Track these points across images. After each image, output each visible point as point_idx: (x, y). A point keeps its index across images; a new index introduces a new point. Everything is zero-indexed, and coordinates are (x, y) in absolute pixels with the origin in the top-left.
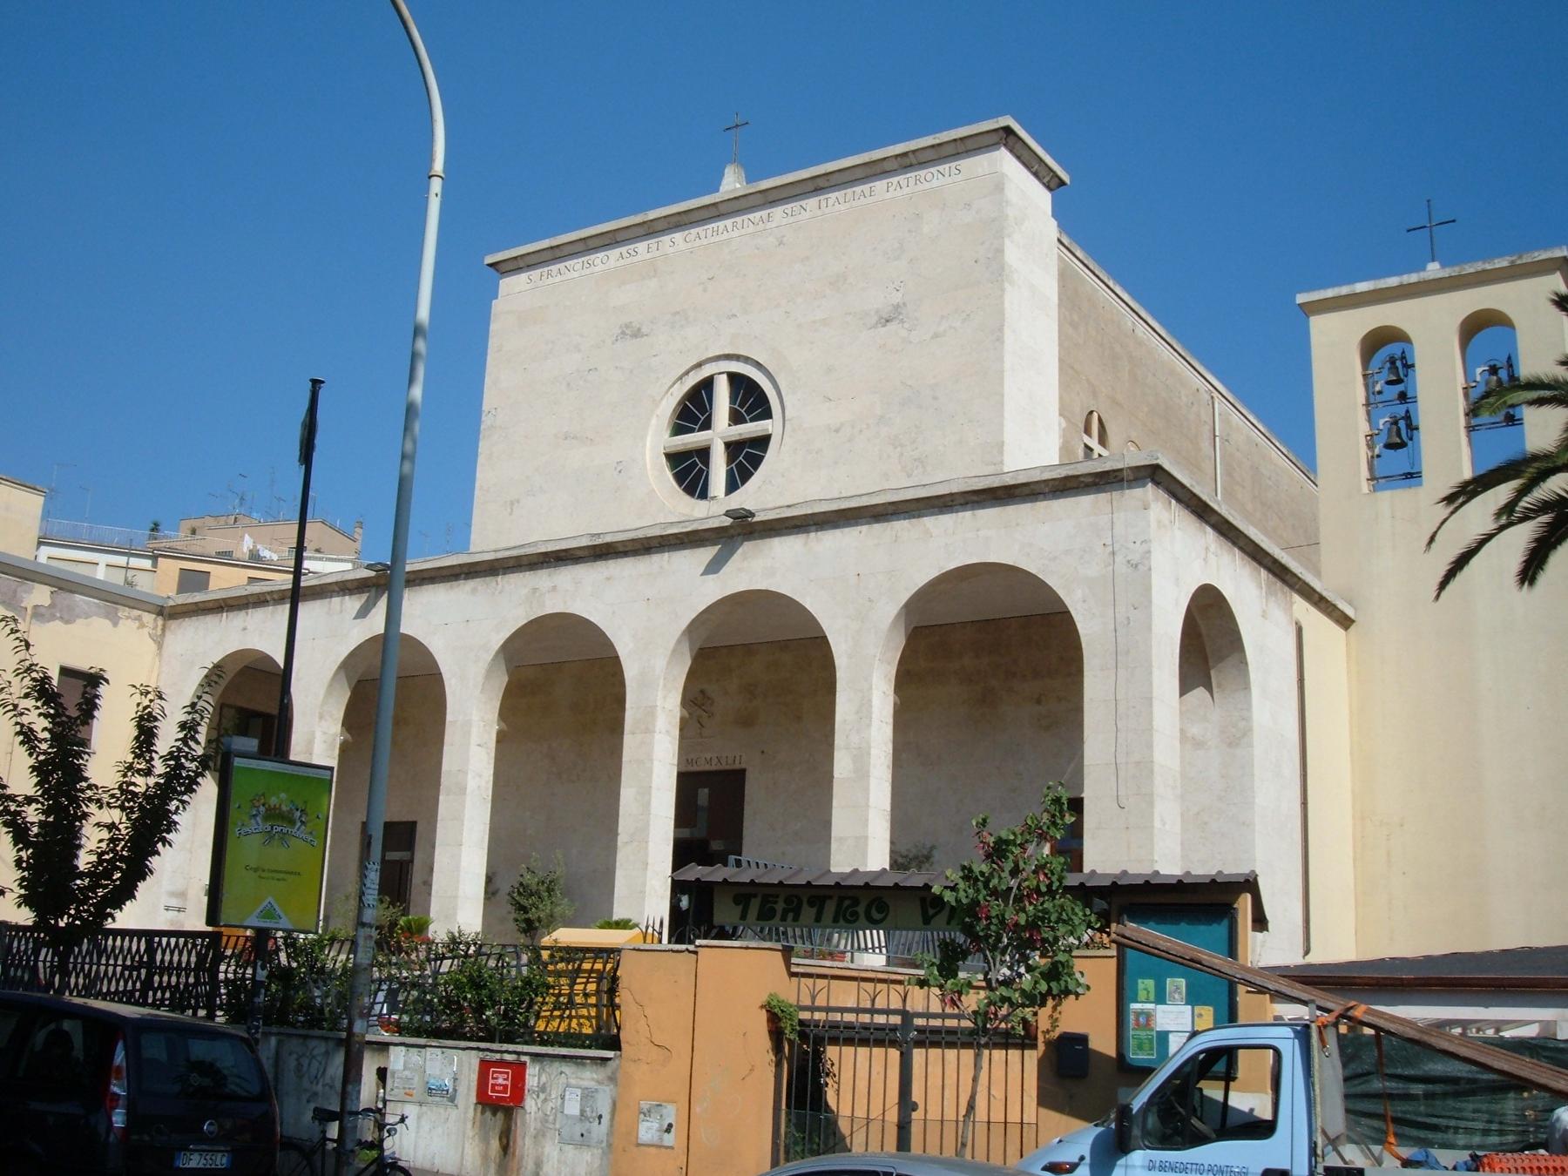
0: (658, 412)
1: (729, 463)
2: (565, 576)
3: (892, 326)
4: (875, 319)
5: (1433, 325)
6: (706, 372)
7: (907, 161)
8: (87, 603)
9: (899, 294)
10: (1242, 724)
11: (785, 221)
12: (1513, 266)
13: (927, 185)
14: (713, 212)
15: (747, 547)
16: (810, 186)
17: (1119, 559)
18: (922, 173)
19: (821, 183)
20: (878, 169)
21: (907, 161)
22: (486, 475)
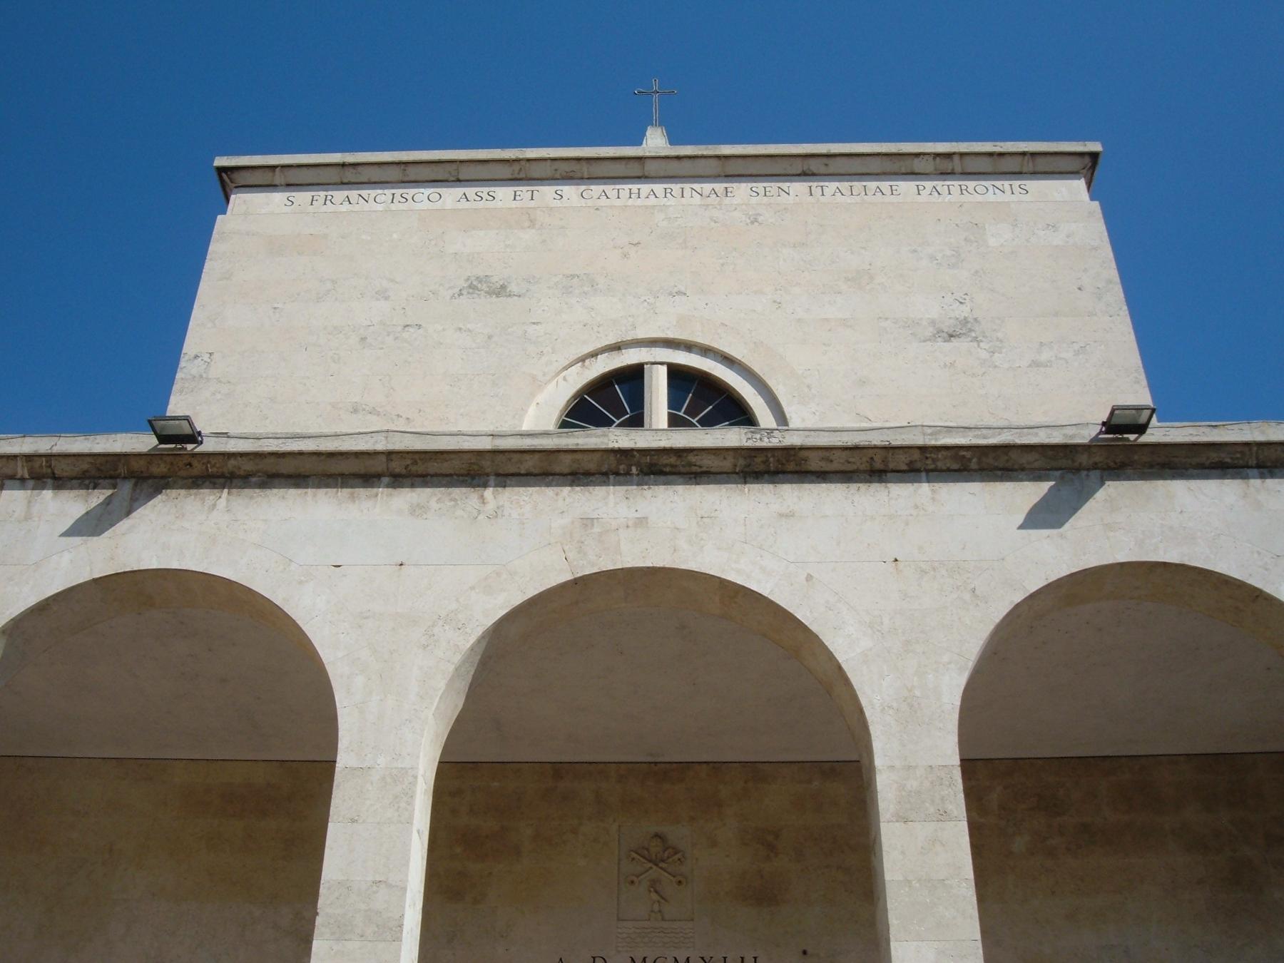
0: (540, 398)
3: (962, 344)
4: (930, 331)
6: (630, 357)
11: (754, 200)
13: (979, 198)
15: (1113, 492)
16: (798, 166)
18: (971, 184)
19: (814, 165)
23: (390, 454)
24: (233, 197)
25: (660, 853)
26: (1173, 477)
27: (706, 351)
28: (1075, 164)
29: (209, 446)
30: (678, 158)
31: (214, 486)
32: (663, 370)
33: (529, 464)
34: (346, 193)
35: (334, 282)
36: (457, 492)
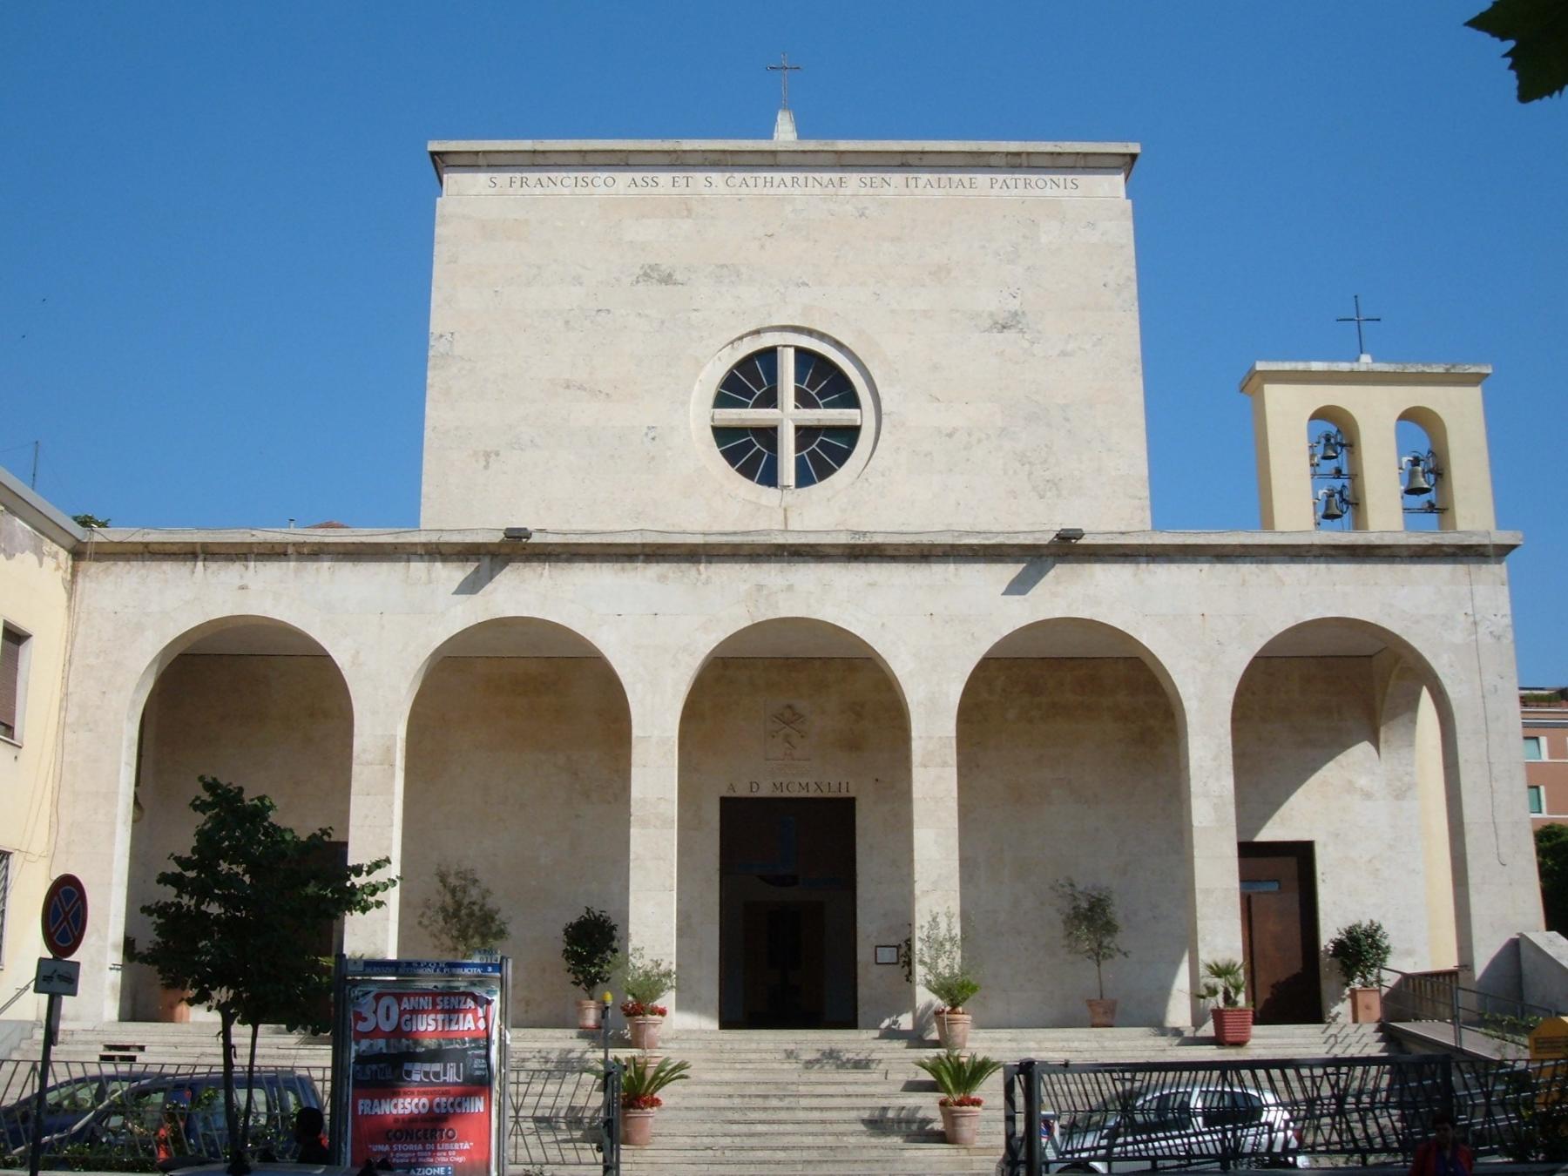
1: (798, 449)
2: (806, 575)
3: (1010, 335)
4: (989, 322)
5: (1376, 413)
7: (1017, 161)
8: (23, 530)
9: (1017, 302)
10: (1406, 779)
11: (863, 191)
12: (1447, 373)
14: (769, 160)
15: (1060, 571)
17: (1481, 629)
18: (1034, 178)
19: (912, 160)
20: (984, 160)
21: (1017, 161)
22: (437, 414)
23: (644, 545)
24: (445, 176)
25: (790, 718)
26: (1096, 562)
27: (822, 337)
28: (1120, 161)
29: (536, 539)
30: (804, 152)
31: (539, 560)
32: (791, 351)
33: (725, 550)
34: (538, 175)
35: (539, 267)
36: (685, 566)
